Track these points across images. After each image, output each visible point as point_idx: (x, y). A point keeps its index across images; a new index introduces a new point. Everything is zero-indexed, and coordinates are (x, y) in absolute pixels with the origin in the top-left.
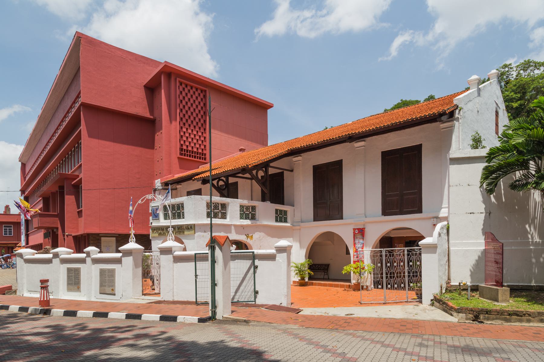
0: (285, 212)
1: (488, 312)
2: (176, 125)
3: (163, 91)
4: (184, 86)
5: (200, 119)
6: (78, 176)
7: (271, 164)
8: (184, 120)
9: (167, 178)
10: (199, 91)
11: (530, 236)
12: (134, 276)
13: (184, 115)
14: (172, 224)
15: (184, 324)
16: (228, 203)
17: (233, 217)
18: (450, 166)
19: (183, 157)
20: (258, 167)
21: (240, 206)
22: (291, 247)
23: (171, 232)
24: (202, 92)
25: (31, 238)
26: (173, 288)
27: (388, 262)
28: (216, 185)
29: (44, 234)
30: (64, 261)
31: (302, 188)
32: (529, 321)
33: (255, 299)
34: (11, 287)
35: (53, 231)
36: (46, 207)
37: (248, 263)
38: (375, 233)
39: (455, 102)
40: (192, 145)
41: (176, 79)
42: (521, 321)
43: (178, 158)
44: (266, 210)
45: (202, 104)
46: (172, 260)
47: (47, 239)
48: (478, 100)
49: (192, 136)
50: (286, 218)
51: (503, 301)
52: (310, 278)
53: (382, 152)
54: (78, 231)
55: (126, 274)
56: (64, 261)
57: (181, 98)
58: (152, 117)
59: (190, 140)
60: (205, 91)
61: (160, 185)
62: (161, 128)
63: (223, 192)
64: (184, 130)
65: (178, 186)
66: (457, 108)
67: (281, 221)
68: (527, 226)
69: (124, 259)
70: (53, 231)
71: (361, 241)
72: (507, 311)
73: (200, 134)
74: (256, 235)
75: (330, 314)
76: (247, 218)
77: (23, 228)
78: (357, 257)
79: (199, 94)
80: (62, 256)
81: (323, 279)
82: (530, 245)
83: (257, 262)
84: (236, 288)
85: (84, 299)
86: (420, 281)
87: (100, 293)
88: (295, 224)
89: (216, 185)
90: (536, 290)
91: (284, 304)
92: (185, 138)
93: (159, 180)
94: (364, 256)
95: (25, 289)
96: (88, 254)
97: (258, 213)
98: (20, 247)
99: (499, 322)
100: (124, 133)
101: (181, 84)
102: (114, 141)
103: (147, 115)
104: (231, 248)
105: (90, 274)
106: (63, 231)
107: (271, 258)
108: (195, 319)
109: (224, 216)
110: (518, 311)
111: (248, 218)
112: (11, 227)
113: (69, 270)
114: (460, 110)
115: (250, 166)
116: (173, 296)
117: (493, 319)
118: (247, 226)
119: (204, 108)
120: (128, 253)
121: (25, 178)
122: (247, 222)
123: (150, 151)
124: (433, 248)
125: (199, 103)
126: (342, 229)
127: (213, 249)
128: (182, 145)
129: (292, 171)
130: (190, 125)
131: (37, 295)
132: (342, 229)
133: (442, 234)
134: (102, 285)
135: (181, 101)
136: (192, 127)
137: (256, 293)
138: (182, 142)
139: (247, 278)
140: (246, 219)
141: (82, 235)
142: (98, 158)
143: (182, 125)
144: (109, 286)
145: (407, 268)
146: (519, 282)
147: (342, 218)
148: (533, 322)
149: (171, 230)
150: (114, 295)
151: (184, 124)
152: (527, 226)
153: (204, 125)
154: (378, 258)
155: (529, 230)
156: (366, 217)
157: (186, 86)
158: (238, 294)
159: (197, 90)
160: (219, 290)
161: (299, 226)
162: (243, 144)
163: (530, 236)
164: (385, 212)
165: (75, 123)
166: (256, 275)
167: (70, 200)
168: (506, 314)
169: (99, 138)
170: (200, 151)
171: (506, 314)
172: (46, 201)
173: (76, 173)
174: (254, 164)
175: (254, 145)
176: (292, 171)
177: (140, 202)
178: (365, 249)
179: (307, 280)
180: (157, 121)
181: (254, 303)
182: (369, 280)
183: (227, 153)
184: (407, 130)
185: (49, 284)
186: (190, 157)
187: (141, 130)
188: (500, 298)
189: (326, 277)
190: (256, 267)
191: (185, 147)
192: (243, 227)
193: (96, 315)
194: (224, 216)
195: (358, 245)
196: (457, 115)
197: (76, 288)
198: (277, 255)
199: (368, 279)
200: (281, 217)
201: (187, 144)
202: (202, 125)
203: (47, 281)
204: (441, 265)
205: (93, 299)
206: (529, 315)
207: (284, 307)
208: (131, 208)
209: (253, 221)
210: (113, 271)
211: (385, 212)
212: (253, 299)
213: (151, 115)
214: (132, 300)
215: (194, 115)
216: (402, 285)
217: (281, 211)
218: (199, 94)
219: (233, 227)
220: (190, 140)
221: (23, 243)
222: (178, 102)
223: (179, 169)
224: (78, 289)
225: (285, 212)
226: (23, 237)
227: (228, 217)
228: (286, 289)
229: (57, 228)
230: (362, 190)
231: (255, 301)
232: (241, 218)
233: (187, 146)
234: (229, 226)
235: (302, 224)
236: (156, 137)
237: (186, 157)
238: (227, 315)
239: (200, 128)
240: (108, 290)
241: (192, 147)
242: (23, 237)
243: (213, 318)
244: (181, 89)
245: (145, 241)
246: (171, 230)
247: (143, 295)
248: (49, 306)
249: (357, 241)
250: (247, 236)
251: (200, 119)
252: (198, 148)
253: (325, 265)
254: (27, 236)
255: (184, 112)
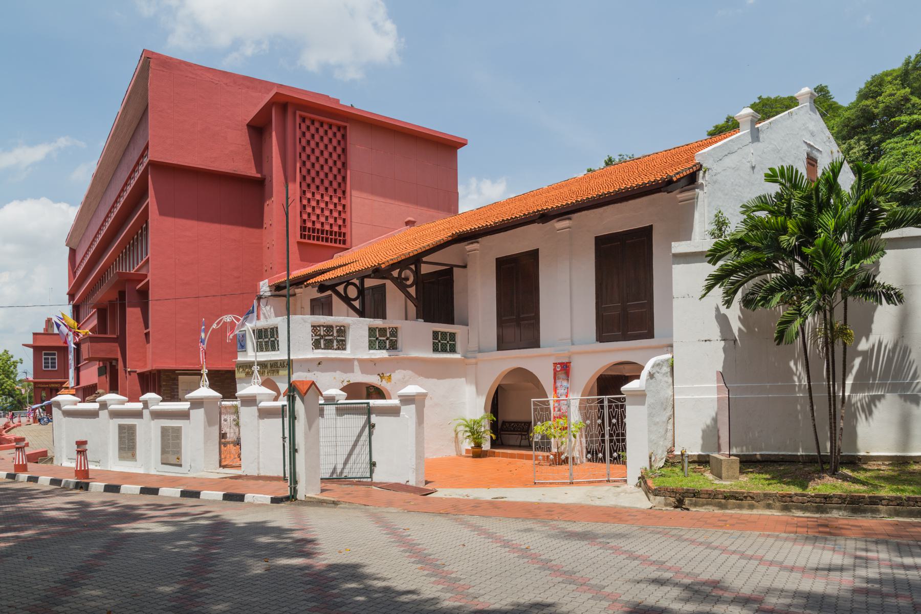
0: (453, 336)
1: (695, 494)
2: (295, 189)
3: (274, 133)
4: (308, 122)
5: (335, 176)
6: (146, 276)
7: (424, 259)
8: (309, 180)
9: (279, 278)
10: (334, 129)
11: (796, 379)
12: (207, 438)
13: (309, 171)
14: (259, 359)
15: (251, 504)
16: (349, 325)
17: (358, 346)
18: (674, 266)
19: (306, 241)
20: (402, 264)
21: (370, 329)
22: (424, 396)
23: (256, 372)
24: (339, 130)
25: (82, 373)
26: (259, 457)
27: (614, 417)
28: (342, 293)
29: (100, 369)
30: (115, 414)
31: (480, 296)
32: (751, 507)
33: (372, 472)
34: (46, 452)
35: (111, 363)
36: (102, 326)
37: (362, 419)
38: (587, 369)
39: (697, 160)
40: (322, 219)
41: (295, 114)
42: (740, 507)
43: (299, 243)
44: (416, 336)
45: (339, 150)
46: (257, 414)
47: (104, 377)
48: (752, 148)
49: (322, 205)
50: (454, 345)
51: (728, 478)
52: (494, 444)
53: (596, 238)
54: (145, 365)
55: (195, 434)
56: (115, 414)
57: (304, 142)
58: (259, 176)
59: (318, 211)
60: (345, 128)
61: (268, 289)
62: (271, 196)
63: (409, 290)
64: (309, 195)
65: (298, 291)
66: (700, 169)
67: (444, 350)
68: (792, 364)
69: (193, 413)
70: (111, 363)
71: (565, 383)
72: (722, 493)
73: (335, 200)
74: (397, 375)
75: (471, 498)
76: (382, 347)
77: (71, 357)
78: (559, 410)
79: (335, 134)
80: (113, 407)
81: (520, 447)
82: (795, 393)
83: (374, 419)
84: (345, 457)
85: (141, 471)
86: (624, 449)
87: (162, 464)
88: (469, 355)
89: (342, 293)
90: (804, 463)
91: (412, 483)
92: (309, 210)
93: (266, 281)
94: (568, 409)
95: (64, 456)
96: (146, 404)
97: (401, 339)
98: (67, 388)
99: (711, 508)
100: (224, 197)
101: (304, 119)
102: (199, 218)
103: (252, 172)
104: (318, 400)
105: (149, 433)
106: (125, 366)
107: (394, 412)
108: (267, 499)
109: (342, 346)
110: (737, 493)
111: (384, 348)
112: (54, 354)
113: (121, 427)
114: (705, 172)
115: (383, 266)
116: (259, 469)
117: (703, 505)
118: (382, 360)
119: (342, 156)
120: (197, 403)
121: (75, 273)
122: (383, 354)
123: (256, 231)
124: (640, 396)
125: (335, 148)
126: (537, 362)
127: (291, 399)
128: (305, 221)
129: (465, 267)
130: (318, 187)
131: (73, 465)
132: (537, 362)
133: (657, 375)
134: (164, 451)
135: (304, 149)
136: (322, 190)
137: (373, 464)
138: (305, 217)
139: (360, 443)
140: (380, 348)
141: (150, 372)
142: (175, 246)
143: (304, 187)
144: (174, 453)
145: (607, 428)
146: (779, 449)
147: (538, 346)
148: (757, 508)
149: (256, 368)
150: (180, 465)
151: (309, 186)
152: (792, 364)
153: (342, 185)
154: (594, 412)
155: (794, 369)
156: (573, 344)
157: (313, 122)
158: (348, 466)
159: (331, 128)
160: (300, 458)
161: (475, 358)
162: (412, 212)
163: (796, 379)
164: (601, 338)
165: (140, 193)
166: (373, 437)
167: (133, 314)
168: (720, 496)
169: (174, 216)
170: (336, 229)
171: (720, 496)
172: (102, 314)
173: (143, 272)
174: (391, 262)
175: (432, 212)
176: (465, 267)
177: (215, 326)
178: (571, 396)
179: (486, 446)
180: (267, 182)
181: (369, 480)
182: (578, 448)
183: (382, 233)
184: (630, 202)
185: (87, 447)
186: (318, 240)
187: (242, 197)
188: (723, 475)
189: (524, 443)
190: (372, 426)
191: (309, 225)
192: (374, 362)
193: (144, 491)
194: (342, 346)
195: (561, 391)
196: (700, 181)
197: (130, 454)
198: (403, 408)
199: (576, 447)
200: (443, 343)
201: (314, 218)
202: (339, 184)
203: (85, 443)
204: (656, 424)
205: (153, 472)
206: (752, 498)
207: (412, 487)
208: (203, 335)
209: (393, 352)
210: (178, 430)
211: (601, 338)
212: (368, 475)
213: (258, 172)
214: (202, 473)
215: (326, 169)
216: (600, 455)
217: (444, 334)
218: (335, 134)
219: (356, 363)
220: (318, 211)
221: (71, 382)
222: (299, 149)
223: (300, 262)
224: (133, 457)
225: (453, 336)
226: (72, 372)
227: (348, 346)
228: (414, 460)
229: (117, 360)
230: (568, 296)
231: (371, 477)
232: (371, 347)
233: (314, 222)
234: (351, 361)
235: (479, 355)
236: (266, 209)
237: (311, 241)
238: (314, 494)
239: (335, 191)
240: (172, 459)
241: (322, 224)
242: (72, 372)
243: (292, 498)
244: (304, 128)
245: (224, 382)
246: (256, 368)
247: (220, 466)
248: (88, 478)
249: (558, 384)
250: (382, 376)
251: (335, 176)
252: (331, 225)
253: (525, 423)
254: (78, 370)
255: (308, 165)
